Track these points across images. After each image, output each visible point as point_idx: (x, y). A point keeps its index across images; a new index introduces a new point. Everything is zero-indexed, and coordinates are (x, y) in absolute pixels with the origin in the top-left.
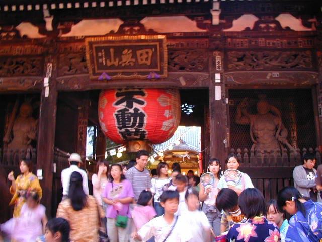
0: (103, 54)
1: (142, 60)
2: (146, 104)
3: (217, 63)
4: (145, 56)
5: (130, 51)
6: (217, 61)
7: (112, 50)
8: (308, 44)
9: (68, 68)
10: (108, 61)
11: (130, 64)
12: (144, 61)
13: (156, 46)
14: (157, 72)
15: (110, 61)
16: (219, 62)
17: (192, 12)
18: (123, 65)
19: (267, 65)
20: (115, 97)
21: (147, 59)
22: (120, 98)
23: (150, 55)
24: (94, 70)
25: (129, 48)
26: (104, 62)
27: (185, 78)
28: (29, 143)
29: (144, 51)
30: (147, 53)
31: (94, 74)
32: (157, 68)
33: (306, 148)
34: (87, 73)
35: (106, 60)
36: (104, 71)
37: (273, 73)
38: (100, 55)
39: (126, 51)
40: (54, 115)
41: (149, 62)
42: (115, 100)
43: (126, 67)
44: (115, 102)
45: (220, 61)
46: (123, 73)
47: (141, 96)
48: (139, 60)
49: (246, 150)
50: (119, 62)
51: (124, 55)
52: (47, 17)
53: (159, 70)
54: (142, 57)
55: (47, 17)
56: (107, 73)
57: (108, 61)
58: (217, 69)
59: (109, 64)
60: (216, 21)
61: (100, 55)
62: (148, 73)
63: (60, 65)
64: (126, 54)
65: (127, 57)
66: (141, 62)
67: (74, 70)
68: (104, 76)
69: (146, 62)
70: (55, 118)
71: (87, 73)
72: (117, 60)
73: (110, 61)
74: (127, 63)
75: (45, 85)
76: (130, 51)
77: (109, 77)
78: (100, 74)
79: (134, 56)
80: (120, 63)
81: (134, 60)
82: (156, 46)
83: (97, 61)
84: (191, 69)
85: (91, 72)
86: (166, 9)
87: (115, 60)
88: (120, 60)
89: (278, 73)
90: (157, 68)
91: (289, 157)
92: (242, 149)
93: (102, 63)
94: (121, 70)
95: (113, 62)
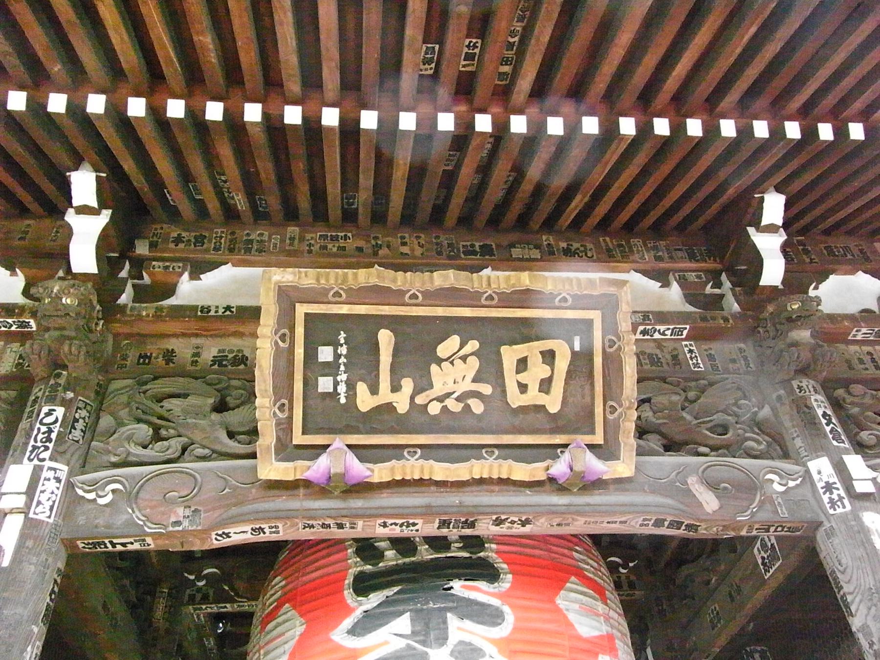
0: (343, 350)
1: (523, 388)
2: (510, 617)
4: (538, 371)
5: (473, 345)
6: (820, 412)
7: (385, 338)
9: (144, 431)
10: (362, 388)
11: (467, 407)
12: (533, 396)
13: (589, 323)
15: (374, 390)
16: (825, 415)
17: (658, 259)
18: (434, 409)
20: (348, 595)
21: (546, 385)
22: (375, 599)
23: (562, 363)
24: (285, 427)
25: (465, 328)
26: (342, 388)
27: (713, 486)
29: (532, 350)
30: (549, 357)
31: (286, 450)
32: (592, 432)
35: (351, 386)
36: (339, 442)
38: (325, 354)
39: (454, 341)
41: (553, 403)
42: (349, 611)
43: (447, 422)
44: (348, 623)
47: (482, 585)
48: (512, 388)
50: (412, 398)
51: (439, 361)
52: (84, 210)
53: (598, 438)
54: (523, 377)
55: (84, 210)
57: (362, 388)
59: (365, 401)
60: (773, 272)
61: (325, 354)
62: (553, 451)
63: (106, 421)
64: (450, 360)
65: (454, 375)
66: (516, 399)
67: (175, 445)
68: (338, 459)
69: (542, 399)
72: (408, 385)
73: (374, 390)
74: (453, 405)
76: (473, 345)
79: (489, 369)
80: (420, 400)
81: (486, 389)
82: (589, 323)
83: (309, 384)
84: (714, 448)
86: (564, 245)
87: (396, 388)
88: (423, 385)
93: (335, 394)
95: (385, 395)
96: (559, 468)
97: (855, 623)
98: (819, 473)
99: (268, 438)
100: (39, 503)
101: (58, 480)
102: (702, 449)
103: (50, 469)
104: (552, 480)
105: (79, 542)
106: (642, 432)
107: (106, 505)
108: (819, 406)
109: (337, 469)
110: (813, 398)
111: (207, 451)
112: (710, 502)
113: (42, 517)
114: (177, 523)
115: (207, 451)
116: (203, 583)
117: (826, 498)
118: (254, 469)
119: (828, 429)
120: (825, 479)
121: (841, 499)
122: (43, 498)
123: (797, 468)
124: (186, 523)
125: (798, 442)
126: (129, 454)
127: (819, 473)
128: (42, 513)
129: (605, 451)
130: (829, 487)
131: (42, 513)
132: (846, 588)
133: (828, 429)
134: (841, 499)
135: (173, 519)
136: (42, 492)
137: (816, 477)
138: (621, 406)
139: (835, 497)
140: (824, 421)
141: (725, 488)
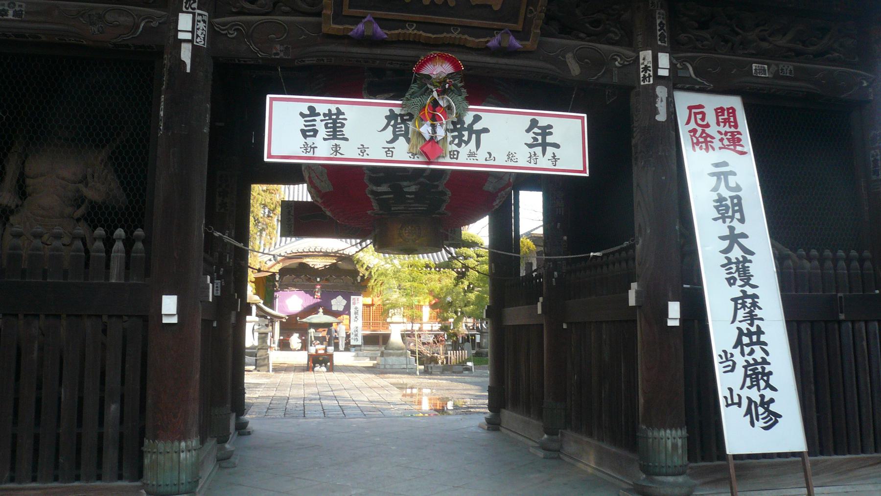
3: (658, 28)
6: (658, 22)
8: (713, 38)
14: (515, 33)
16: (661, 23)
19: (765, 45)
27: (579, 59)
28: (79, 213)
31: (338, 17)
33: (818, 250)
34: (319, 14)
37: (781, 66)
40: (206, 130)
45: (664, 22)
46: (420, 25)
49: (120, 232)
53: (519, 27)
56: (378, 20)
58: (659, 43)
62: (489, 32)
70: (207, 140)
71: (319, 14)
75: (181, 36)
77: (381, 33)
78: (357, 20)
84: (589, 35)
85: (328, 12)
89: (791, 67)
90: (516, 23)
91: (835, 270)
92: (129, 232)
94: (418, 17)
96: (493, 42)
97: (633, 142)
98: (644, 59)
99: (328, 12)
100: (198, 36)
101: (204, 22)
102: (582, 35)
103: (199, 14)
104: (487, 48)
105: (450, 214)
106: (549, 18)
107: (233, 38)
108: (659, 18)
109: (368, 33)
110: (658, 11)
111: (288, 9)
112: (575, 69)
113: (201, 44)
114: (277, 54)
115: (288, 9)
116: (413, 189)
117: (642, 75)
118: (319, 25)
119: (659, 33)
120: (646, 63)
121: (649, 76)
122: (199, 32)
123: (633, 54)
124: (282, 54)
125: (640, 38)
126: (243, 7)
127: (644, 59)
128: (200, 42)
129: (521, 35)
130: (646, 69)
131: (200, 42)
132: (636, 124)
133: (659, 33)
134: (649, 76)
135: (274, 51)
136: (198, 29)
137: (641, 61)
138: (536, 10)
139: (647, 75)
140: (658, 28)
141: (587, 63)
